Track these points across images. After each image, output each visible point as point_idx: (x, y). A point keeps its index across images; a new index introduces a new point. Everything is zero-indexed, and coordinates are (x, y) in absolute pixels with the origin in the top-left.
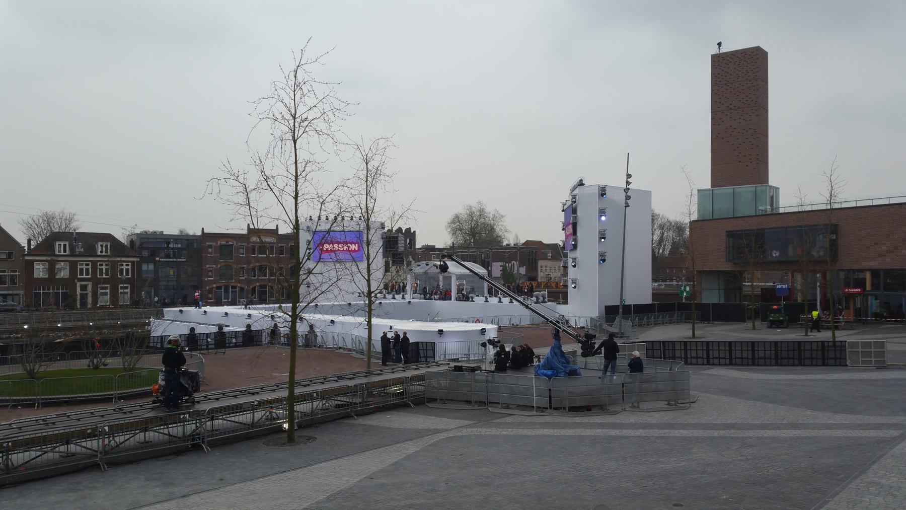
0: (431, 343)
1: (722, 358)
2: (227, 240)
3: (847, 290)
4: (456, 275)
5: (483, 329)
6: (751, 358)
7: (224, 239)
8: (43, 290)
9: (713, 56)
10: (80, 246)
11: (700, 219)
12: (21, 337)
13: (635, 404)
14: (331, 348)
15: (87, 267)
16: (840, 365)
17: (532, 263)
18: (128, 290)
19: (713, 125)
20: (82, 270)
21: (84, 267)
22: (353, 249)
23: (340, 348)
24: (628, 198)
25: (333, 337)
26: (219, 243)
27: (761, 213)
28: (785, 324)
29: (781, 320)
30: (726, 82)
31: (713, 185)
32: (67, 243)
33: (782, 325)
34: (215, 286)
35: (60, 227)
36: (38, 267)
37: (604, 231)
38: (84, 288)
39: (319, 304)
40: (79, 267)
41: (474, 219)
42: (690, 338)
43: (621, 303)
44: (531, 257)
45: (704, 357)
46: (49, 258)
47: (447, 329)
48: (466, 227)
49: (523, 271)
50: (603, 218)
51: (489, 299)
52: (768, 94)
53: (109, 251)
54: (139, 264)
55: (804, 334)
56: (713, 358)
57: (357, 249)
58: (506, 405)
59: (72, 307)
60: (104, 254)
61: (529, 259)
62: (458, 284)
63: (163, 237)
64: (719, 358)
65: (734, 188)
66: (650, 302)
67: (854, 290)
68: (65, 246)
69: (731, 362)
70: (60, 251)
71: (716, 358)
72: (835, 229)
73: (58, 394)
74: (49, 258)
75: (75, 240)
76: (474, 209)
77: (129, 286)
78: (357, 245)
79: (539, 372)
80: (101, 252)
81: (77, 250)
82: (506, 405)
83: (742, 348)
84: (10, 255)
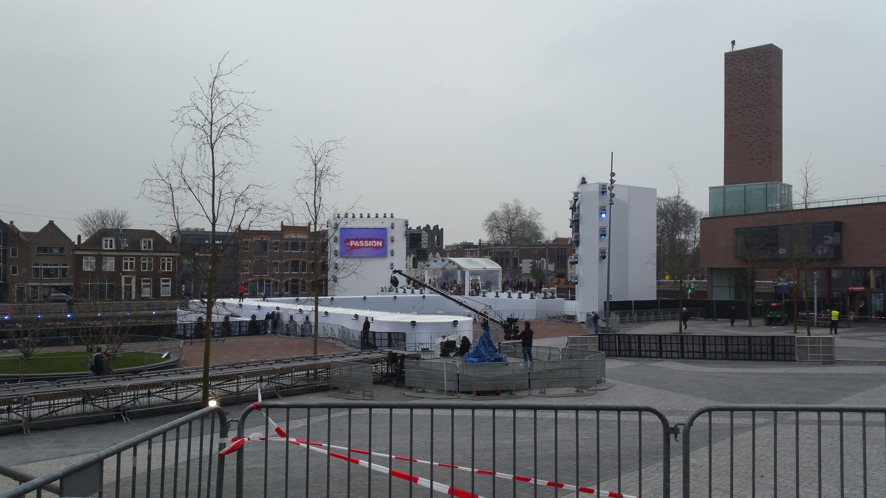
0: (402, 333)
1: (764, 353)
2: (261, 236)
3: (851, 288)
4: (470, 271)
5: (455, 321)
6: (771, 353)
7: (259, 236)
8: (108, 285)
9: (726, 55)
10: (125, 242)
11: (711, 216)
12: (64, 325)
13: (543, 391)
14: (322, 338)
15: (132, 261)
16: (791, 360)
17: (561, 260)
18: (170, 283)
19: (726, 123)
20: (126, 264)
21: (129, 261)
22: (378, 246)
23: (330, 338)
24: (612, 196)
25: (324, 327)
26: (254, 239)
27: (770, 210)
28: (783, 321)
29: (779, 317)
30: (739, 80)
31: (726, 182)
32: (113, 240)
33: (780, 322)
34: (250, 280)
35: (113, 224)
36: (111, 261)
37: (604, 228)
38: (128, 281)
39: (334, 297)
40: (124, 261)
41: (511, 216)
42: (677, 333)
43: (608, 300)
44: (560, 254)
45: (769, 353)
46: (96, 253)
47: (420, 321)
48: (504, 226)
49: (551, 267)
50: (604, 215)
51: (500, 294)
52: (782, 91)
53: (152, 247)
54: (179, 259)
55: (793, 332)
56: (756, 353)
57: (381, 245)
58: (422, 389)
59: (118, 299)
60: (147, 249)
61: (558, 255)
62: (471, 279)
63: (205, 234)
64: (762, 353)
65: (766, 184)
66: (655, 299)
67: (858, 288)
68: (111, 241)
69: (682, 356)
70: (106, 246)
71: (648, 351)
72: (838, 227)
73: (42, 373)
74: (96, 253)
75: (121, 237)
76: (510, 207)
77: (170, 279)
78: (381, 242)
79: (467, 360)
80: (145, 247)
81: (122, 245)
82: (422, 389)
83: (785, 343)
84: (62, 250)
